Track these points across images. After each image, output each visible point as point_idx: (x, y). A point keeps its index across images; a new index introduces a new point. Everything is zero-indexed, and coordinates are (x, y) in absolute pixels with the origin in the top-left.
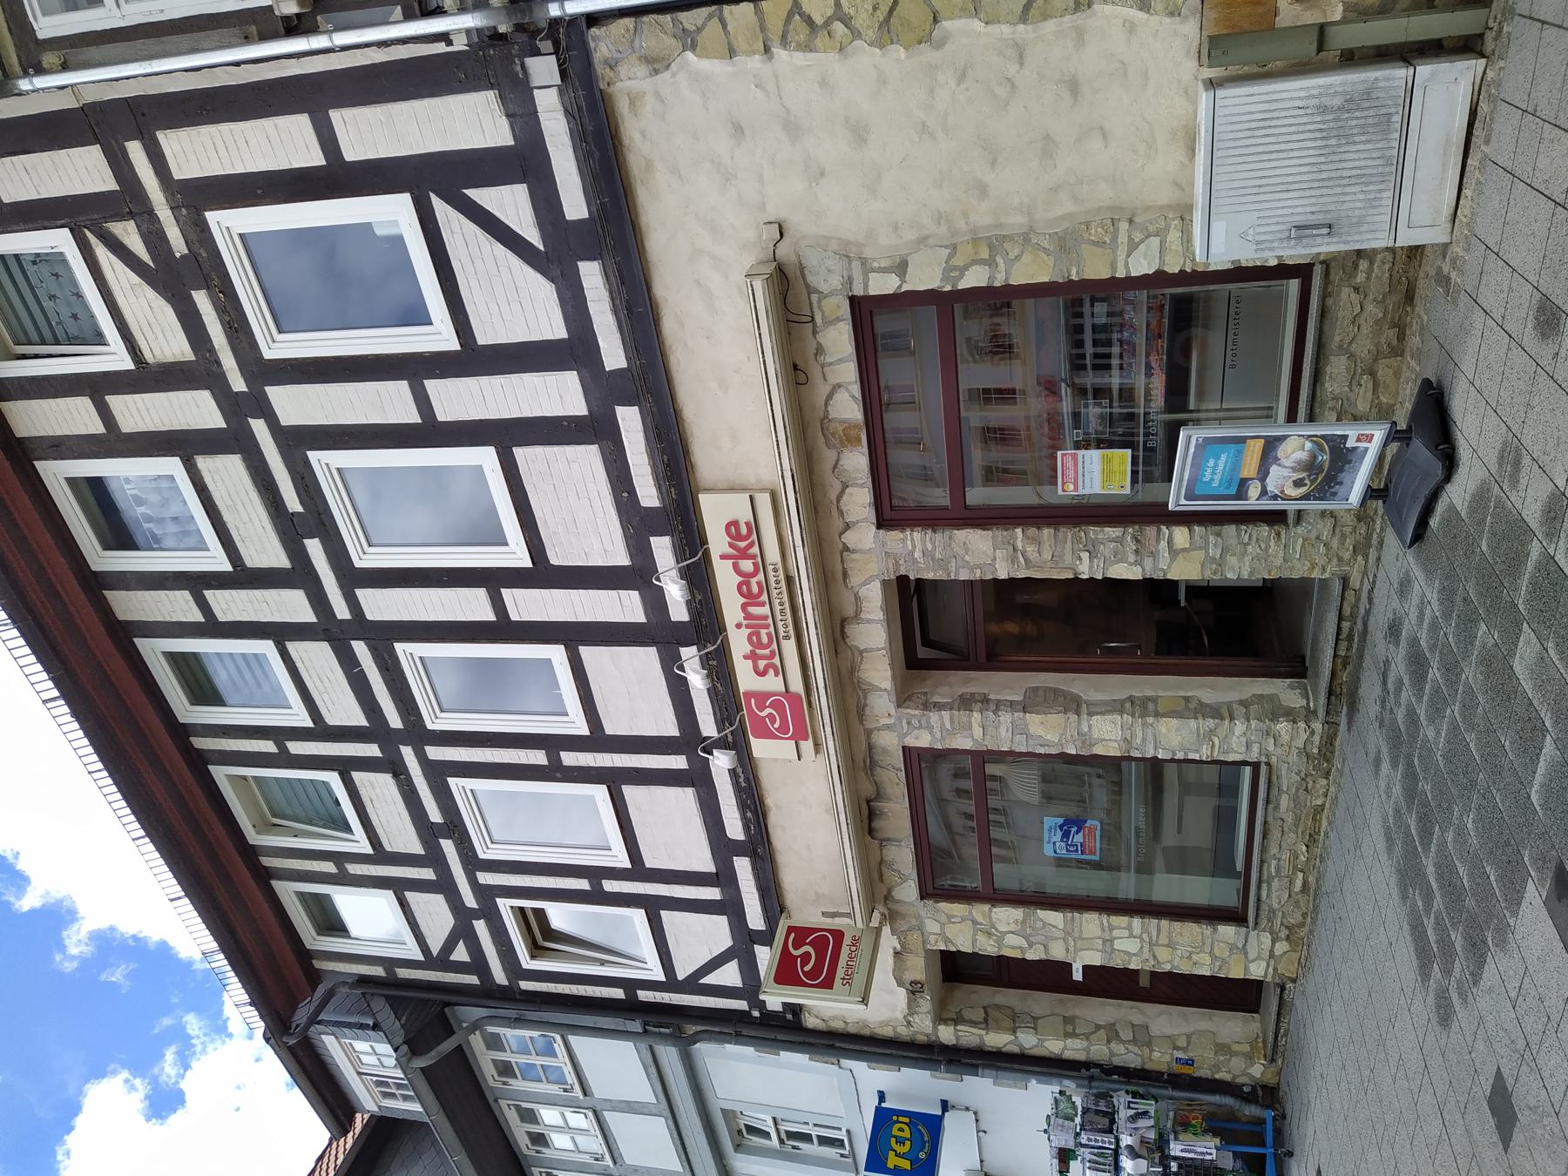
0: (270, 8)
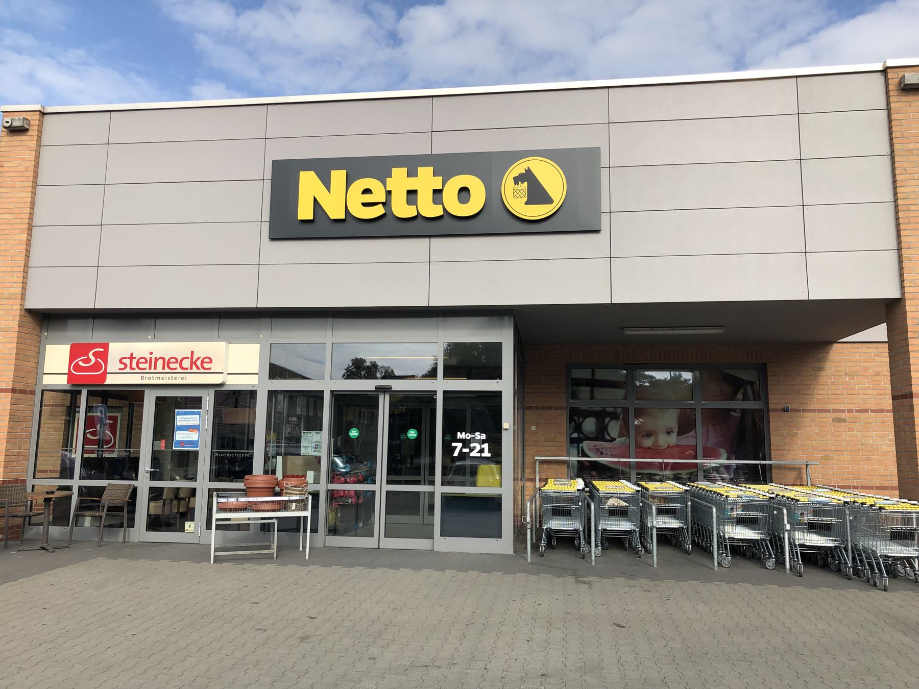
0: (391, 177)
